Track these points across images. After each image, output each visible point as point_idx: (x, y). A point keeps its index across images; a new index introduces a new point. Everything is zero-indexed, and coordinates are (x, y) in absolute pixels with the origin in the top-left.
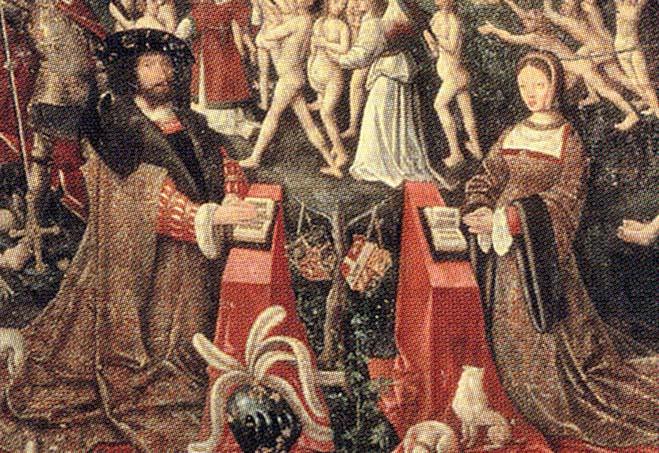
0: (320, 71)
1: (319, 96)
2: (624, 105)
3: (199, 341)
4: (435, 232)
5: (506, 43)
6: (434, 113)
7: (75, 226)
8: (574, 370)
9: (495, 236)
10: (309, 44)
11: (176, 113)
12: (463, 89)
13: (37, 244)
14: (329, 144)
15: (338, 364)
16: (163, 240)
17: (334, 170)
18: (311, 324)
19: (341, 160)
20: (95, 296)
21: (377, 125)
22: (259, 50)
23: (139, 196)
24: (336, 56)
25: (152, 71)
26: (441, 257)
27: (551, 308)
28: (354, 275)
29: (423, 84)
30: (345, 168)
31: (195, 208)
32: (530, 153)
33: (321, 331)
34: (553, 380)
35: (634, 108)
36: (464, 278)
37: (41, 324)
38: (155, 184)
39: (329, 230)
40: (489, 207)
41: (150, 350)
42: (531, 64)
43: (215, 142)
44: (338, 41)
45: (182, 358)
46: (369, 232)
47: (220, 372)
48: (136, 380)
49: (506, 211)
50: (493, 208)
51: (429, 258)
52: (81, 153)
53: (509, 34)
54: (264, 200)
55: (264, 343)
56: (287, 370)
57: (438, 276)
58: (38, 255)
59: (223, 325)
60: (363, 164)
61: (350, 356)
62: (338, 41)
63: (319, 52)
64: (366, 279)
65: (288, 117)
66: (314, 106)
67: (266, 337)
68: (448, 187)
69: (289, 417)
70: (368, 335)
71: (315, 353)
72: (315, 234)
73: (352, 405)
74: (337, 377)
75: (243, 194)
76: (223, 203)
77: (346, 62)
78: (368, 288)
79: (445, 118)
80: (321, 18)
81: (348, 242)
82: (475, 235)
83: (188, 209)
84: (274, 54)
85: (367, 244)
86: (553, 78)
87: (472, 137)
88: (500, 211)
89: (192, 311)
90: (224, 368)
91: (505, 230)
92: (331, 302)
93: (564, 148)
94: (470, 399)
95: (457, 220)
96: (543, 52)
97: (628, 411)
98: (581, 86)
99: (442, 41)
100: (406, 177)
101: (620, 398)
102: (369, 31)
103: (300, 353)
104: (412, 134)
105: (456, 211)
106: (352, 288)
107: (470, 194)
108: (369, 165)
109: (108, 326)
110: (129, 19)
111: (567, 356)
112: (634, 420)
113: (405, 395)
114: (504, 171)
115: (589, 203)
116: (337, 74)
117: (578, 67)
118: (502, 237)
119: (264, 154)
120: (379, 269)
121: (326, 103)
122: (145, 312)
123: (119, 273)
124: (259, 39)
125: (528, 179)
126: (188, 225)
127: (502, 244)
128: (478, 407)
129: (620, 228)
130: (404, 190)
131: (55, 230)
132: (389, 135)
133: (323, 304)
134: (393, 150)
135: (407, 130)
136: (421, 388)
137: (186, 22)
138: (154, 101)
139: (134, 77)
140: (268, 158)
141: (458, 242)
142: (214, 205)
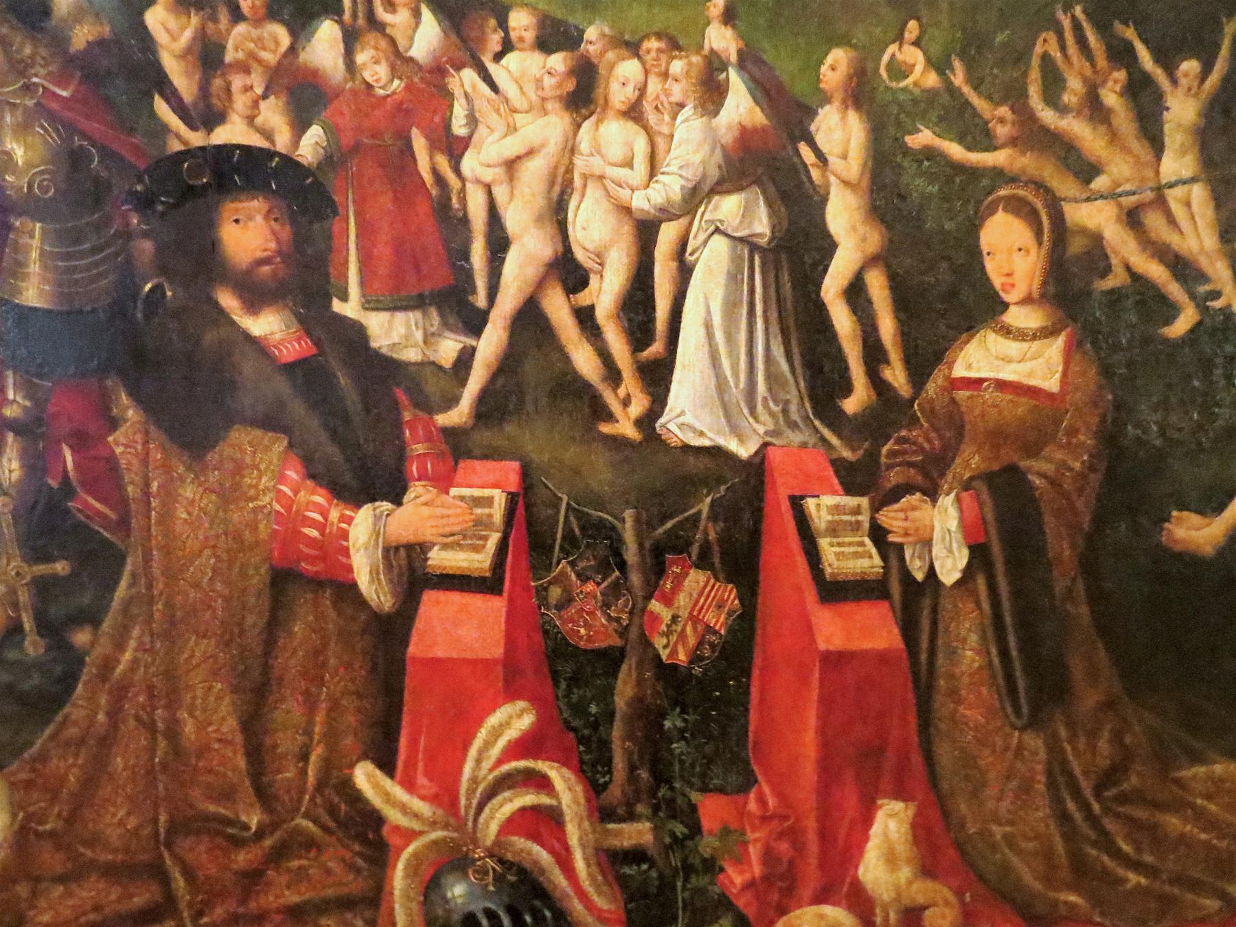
0: (594, 227)
1: (594, 280)
2: (1175, 290)
3: (365, 776)
4: (824, 543)
5: (960, 168)
6: (821, 307)
7: (100, 559)
8: (1076, 792)
9: (936, 551)
10: (569, 170)
11: (301, 320)
12: (871, 261)
13: (24, 597)
14: (613, 375)
15: (640, 808)
16: (283, 580)
17: (625, 427)
18: (586, 732)
19: (638, 406)
20: (152, 696)
21: (710, 335)
22: (468, 185)
23: (230, 495)
24: (624, 194)
25: (247, 232)
26: (836, 591)
27: (1037, 681)
28: (667, 634)
29: (796, 251)
30: (647, 422)
31: (348, 513)
32: (1001, 385)
33: (605, 745)
34: (1040, 814)
35: (1193, 296)
36: (873, 630)
37: (43, 757)
38: (272, 480)
39: (616, 549)
40: (925, 493)
41: (264, 795)
42: (1005, 210)
43: (381, 371)
44: (629, 164)
45: (332, 810)
46: (695, 550)
47: (411, 835)
48: (242, 859)
49: (958, 500)
50: (932, 494)
51: (810, 594)
52: (109, 409)
53: (964, 151)
54: (487, 492)
55: (496, 773)
56: (543, 823)
57: (833, 630)
58: (28, 623)
59: (414, 742)
60: (682, 413)
61: (663, 792)
62: (629, 164)
63: (590, 185)
64: (692, 641)
65: (530, 318)
66: (583, 298)
67: (500, 762)
68: (847, 454)
69: (548, 914)
70: (696, 747)
71: (595, 788)
72: (589, 553)
73: (666, 886)
74: (636, 833)
75: (443, 482)
76: (405, 500)
77: (646, 206)
78: (695, 658)
79: (842, 320)
80: (593, 118)
81: (656, 569)
82: (900, 548)
83: (334, 515)
84: (500, 193)
85: (692, 572)
86: (1046, 238)
87: (895, 355)
88: (947, 502)
89: (351, 719)
90: (416, 826)
91: (957, 537)
92: (624, 690)
93: (1065, 374)
94: (891, 860)
95: (864, 518)
96: (1026, 183)
97: (1170, 865)
98: (1097, 256)
99: (833, 161)
100: (768, 439)
101: (1153, 835)
102: (692, 144)
103: (566, 790)
104: (778, 351)
105: (864, 502)
106: (664, 657)
107: (890, 467)
108: (693, 413)
109: (177, 750)
110: (193, 128)
111: (1070, 775)
112: (1177, 880)
113: (768, 856)
114: (954, 424)
115: (1111, 474)
116: (627, 231)
117: (1094, 216)
118: (950, 551)
119: (484, 396)
120: (718, 620)
121: (606, 291)
122: (254, 726)
123: (197, 649)
124: (468, 164)
125: (997, 437)
126: (334, 548)
127: (951, 564)
128: (905, 873)
129: (1167, 525)
130: (762, 462)
131: (61, 567)
132: (733, 354)
133: (607, 693)
134: (742, 385)
135: (769, 345)
136: (799, 847)
137: (314, 135)
138: (256, 296)
139: (214, 245)
140: (491, 408)
141: (869, 563)
142: (385, 506)
